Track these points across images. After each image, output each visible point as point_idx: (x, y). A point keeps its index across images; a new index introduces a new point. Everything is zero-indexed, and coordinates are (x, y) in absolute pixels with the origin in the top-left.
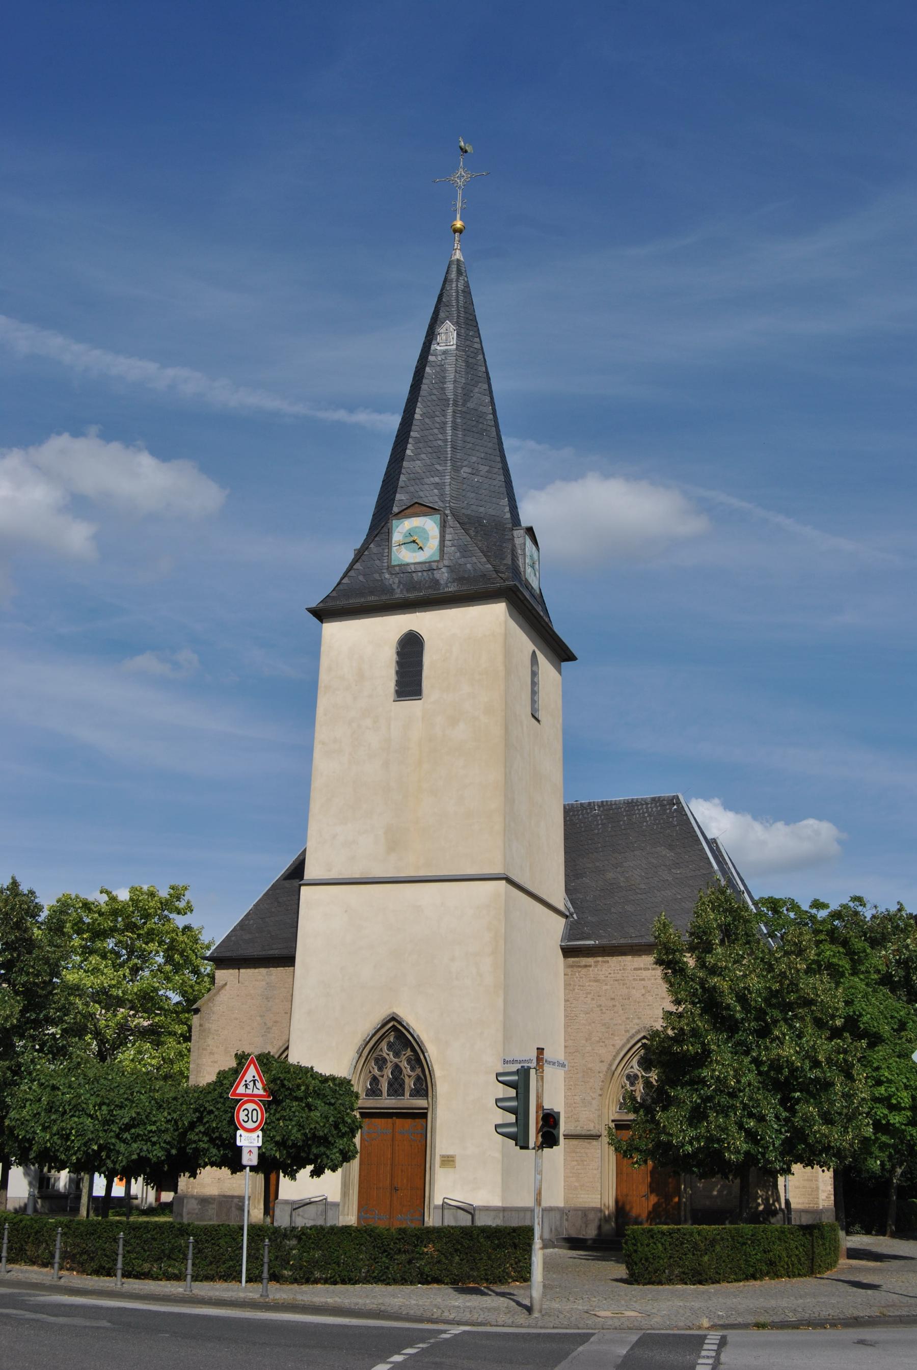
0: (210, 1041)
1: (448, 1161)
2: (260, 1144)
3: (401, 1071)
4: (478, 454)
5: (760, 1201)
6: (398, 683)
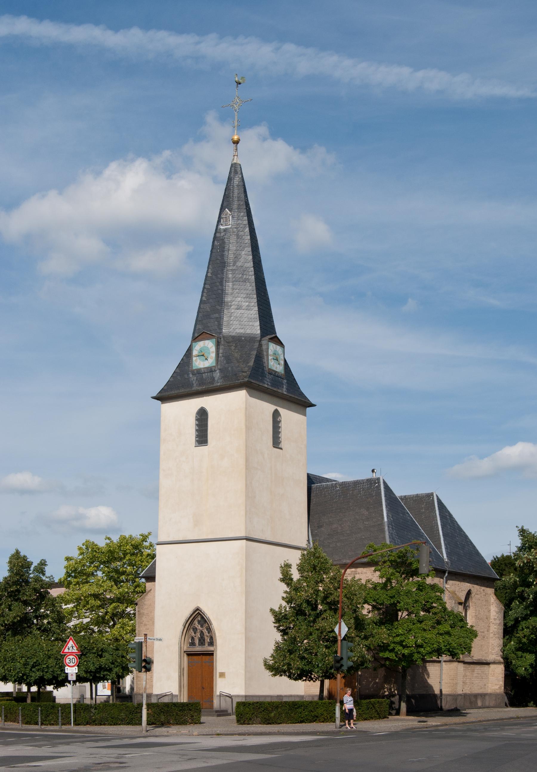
0: (144, 619)
1: (222, 675)
2: (77, 672)
3: (203, 634)
4: (242, 295)
5: (386, 690)
6: (197, 436)
